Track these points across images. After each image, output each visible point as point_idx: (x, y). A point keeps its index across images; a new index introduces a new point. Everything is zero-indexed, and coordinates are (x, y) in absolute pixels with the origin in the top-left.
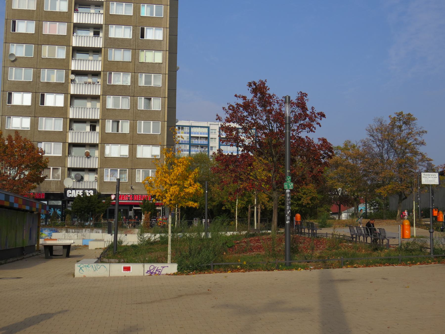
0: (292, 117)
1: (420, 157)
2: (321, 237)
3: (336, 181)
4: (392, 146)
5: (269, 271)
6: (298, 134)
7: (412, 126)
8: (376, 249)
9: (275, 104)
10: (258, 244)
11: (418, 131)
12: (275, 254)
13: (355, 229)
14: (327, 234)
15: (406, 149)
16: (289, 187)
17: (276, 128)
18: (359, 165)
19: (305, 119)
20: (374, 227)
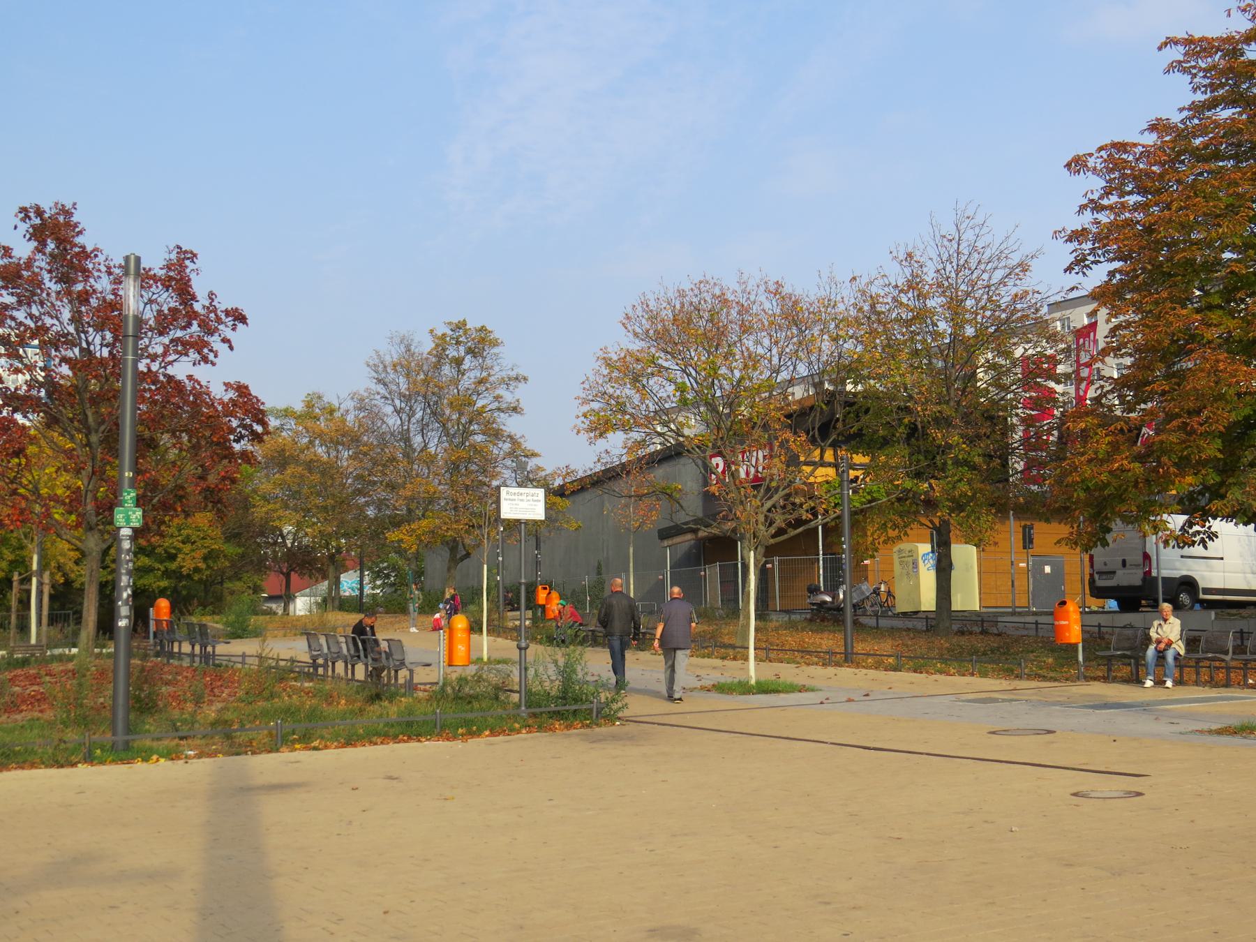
0: (150, 319)
1: (507, 446)
2: (227, 666)
3: (278, 506)
4: (434, 413)
5: (62, 766)
6: (165, 367)
7: (488, 362)
8: (377, 697)
9: (102, 275)
10: (36, 688)
11: (504, 374)
12: (85, 718)
13: (323, 640)
14: (244, 656)
15: (470, 422)
16: (128, 520)
17: (99, 347)
18: (345, 464)
19: (189, 325)
20: (373, 634)
